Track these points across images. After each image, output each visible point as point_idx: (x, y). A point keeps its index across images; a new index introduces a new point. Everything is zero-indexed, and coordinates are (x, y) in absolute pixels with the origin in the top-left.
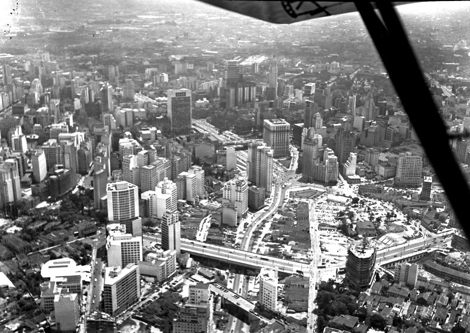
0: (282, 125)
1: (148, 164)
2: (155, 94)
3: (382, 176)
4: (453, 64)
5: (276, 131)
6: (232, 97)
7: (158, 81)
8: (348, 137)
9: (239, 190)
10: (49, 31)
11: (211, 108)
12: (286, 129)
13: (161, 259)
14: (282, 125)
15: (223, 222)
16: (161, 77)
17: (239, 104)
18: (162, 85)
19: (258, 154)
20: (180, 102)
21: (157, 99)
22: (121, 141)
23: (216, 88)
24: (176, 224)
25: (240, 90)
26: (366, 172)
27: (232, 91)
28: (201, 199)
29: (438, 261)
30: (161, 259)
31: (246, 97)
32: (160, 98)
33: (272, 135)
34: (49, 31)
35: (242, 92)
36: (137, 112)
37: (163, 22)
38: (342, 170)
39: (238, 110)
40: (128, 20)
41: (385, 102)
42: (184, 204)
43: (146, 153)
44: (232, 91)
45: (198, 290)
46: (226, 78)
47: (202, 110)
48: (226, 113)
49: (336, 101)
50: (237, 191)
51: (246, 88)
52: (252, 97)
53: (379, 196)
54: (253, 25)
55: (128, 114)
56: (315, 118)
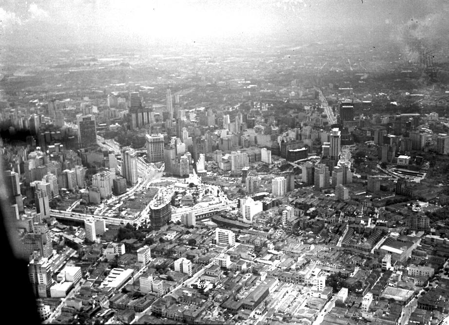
0: (156, 137)
3: (222, 170)
4: (348, 89)
5: (153, 143)
6: (134, 122)
8: (200, 143)
9: (102, 179)
10: (13, 76)
13: (29, 217)
14: (156, 137)
15: (91, 202)
22: (347, 290)
24: (45, 198)
25: (140, 115)
26: (212, 168)
27: (134, 116)
28: (80, 188)
29: (222, 216)
30: (29, 217)
31: (146, 120)
34: (13, 76)
35: (141, 118)
36: (54, 134)
37: (119, 64)
38: (194, 166)
40: (87, 63)
41: (254, 119)
42: (64, 191)
44: (134, 116)
45: (39, 226)
50: (101, 180)
51: (144, 113)
52: (150, 120)
53: (214, 182)
55: (47, 136)
56: (182, 132)
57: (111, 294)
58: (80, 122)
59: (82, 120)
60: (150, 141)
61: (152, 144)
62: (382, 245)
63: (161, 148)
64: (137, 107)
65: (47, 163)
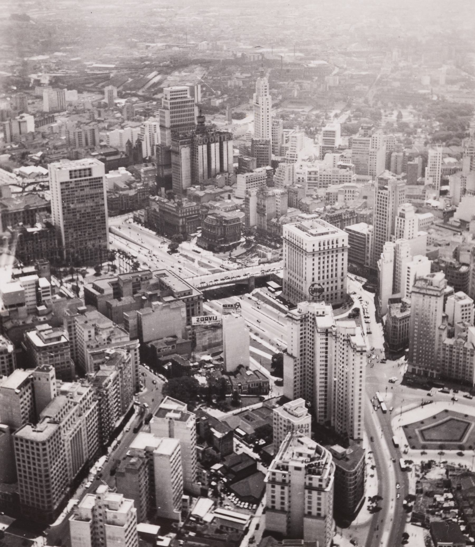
1: (34, 418)
2: (12, 158)
7: (16, 130)
9: (316, 483)
11: (139, 191)
12: (340, 245)
16: (20, 123)
17: (200, 180)
18: (23, 140)
19: (319, 340)
20: (79, 189)
21: (17, 170)
23: (139, 142)
25: (202, 149)
27: (185, 152)
32: (23, 169)
33: (309, 261)
39: (201, 194)
43: (26, 382)
46: (168, 124)
47: (121, 196)
48: (180, 204)
49: (393, 159)
50: (310, 488)
51: (213, 145)
54: (162, 17)
57: (130, 407)
58: (62, 183)
59: (66, 178)
60: (310, 249)
61: (316, 258)
62: (123, 190)
63: (340, 267)
64: (193, 131)
65: (48, 402)
